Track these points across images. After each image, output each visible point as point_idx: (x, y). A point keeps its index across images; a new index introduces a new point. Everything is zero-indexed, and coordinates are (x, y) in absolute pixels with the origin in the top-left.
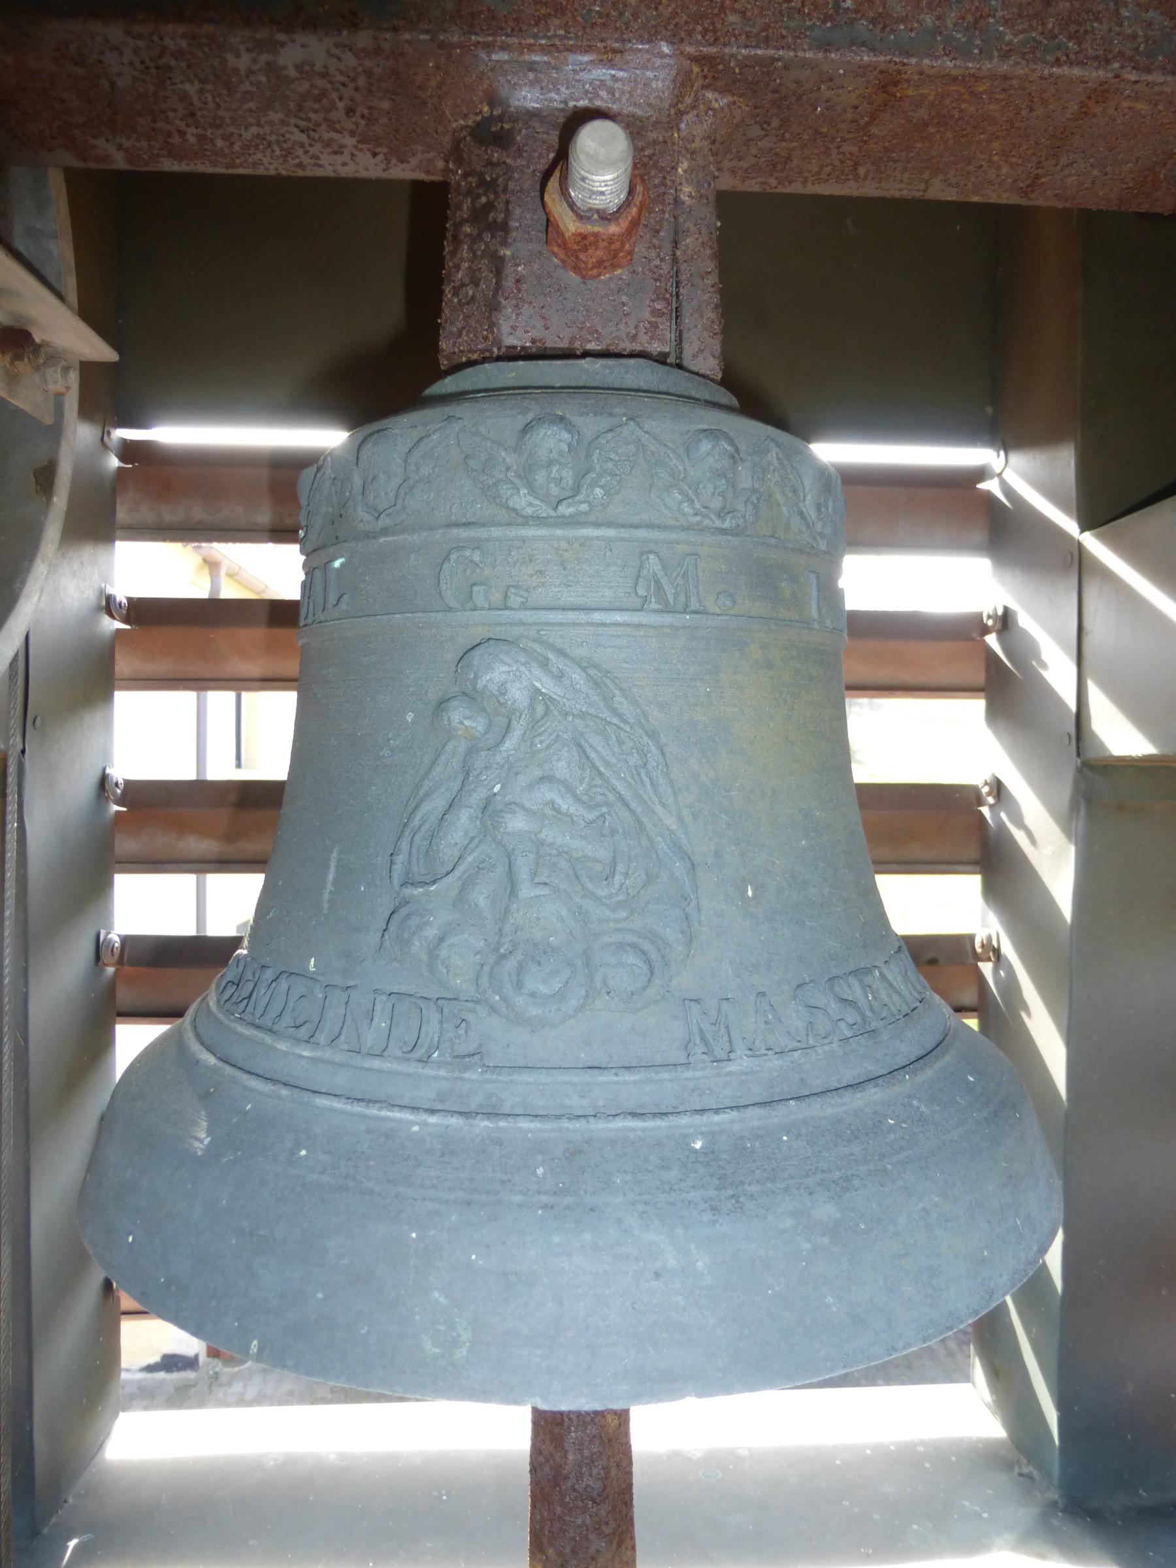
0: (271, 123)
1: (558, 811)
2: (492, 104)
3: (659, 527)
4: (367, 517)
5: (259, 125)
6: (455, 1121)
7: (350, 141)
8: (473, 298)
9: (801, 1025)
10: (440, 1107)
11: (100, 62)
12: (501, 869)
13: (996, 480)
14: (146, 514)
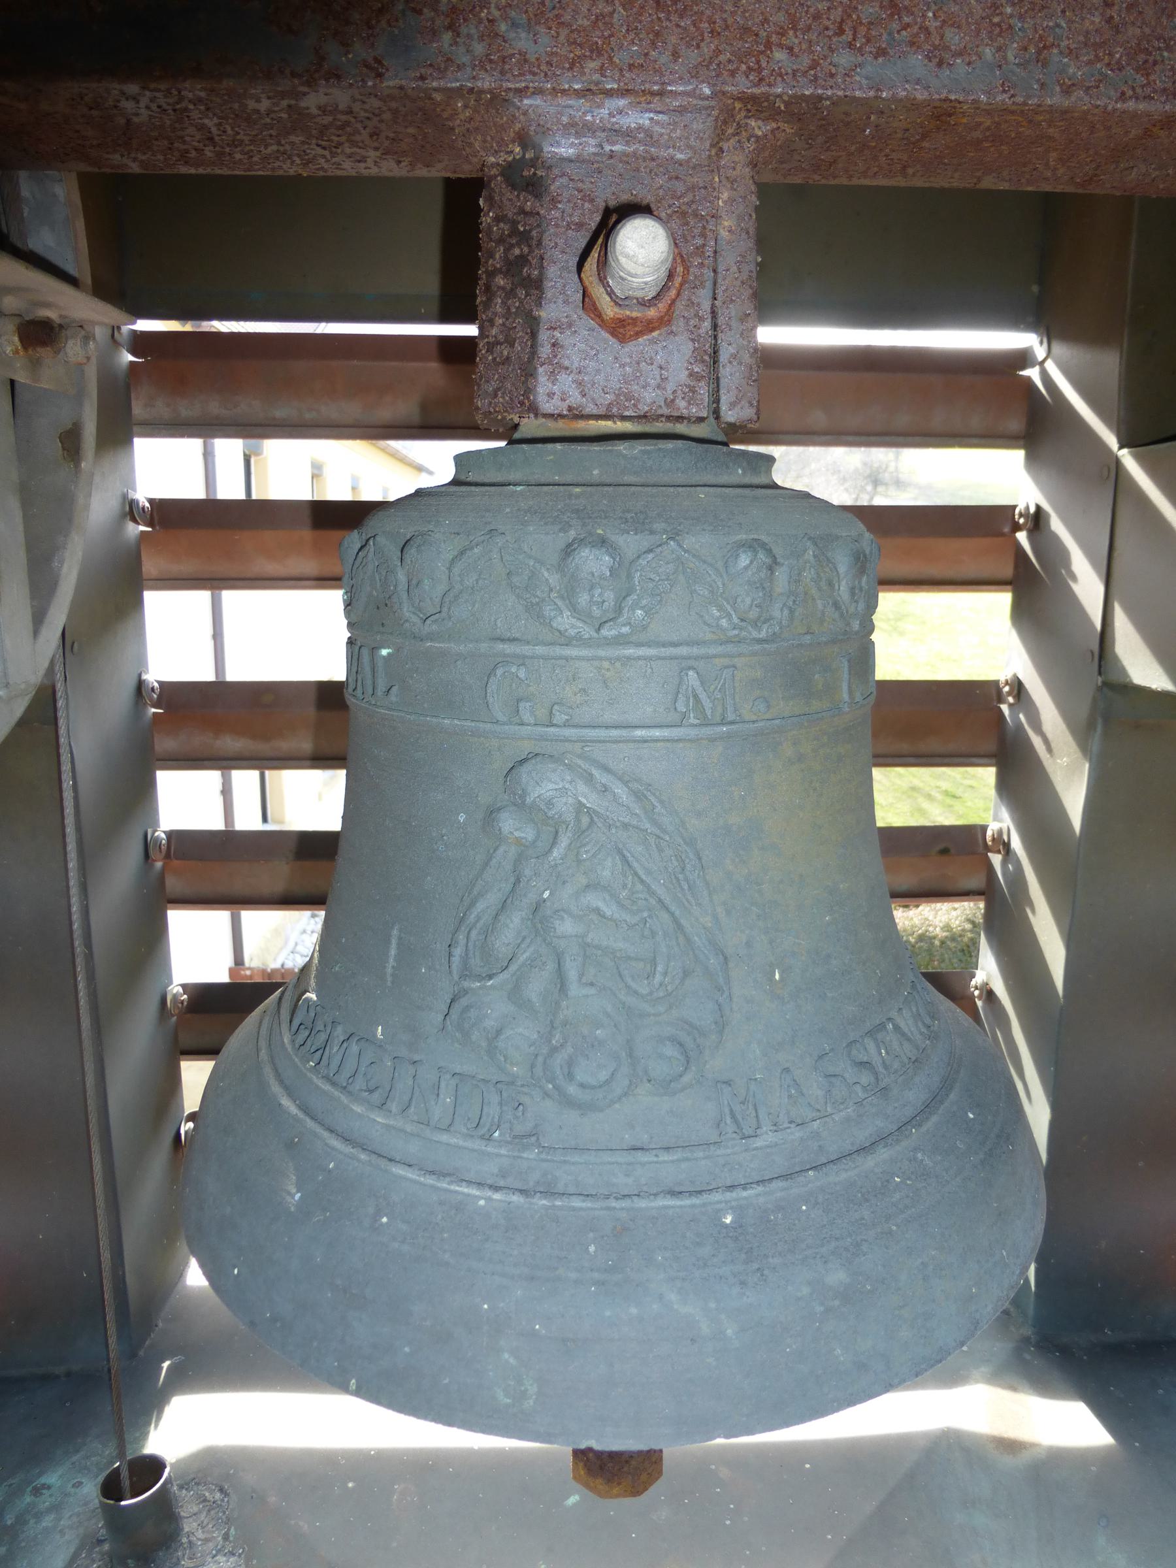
0: (292, 143)
1: (603, 916)
2: (524, 147)
3: (697, 643)
4: (414, 619)
5: (279, 144)
6: (516, 1198)
7: (372, 154)
8: (508, 358)
9: (820, 1093)
10: (502, 1183)
11: (116, 107)
12: (551, 966)
13: (1037, 368)
14: (162, 409)
